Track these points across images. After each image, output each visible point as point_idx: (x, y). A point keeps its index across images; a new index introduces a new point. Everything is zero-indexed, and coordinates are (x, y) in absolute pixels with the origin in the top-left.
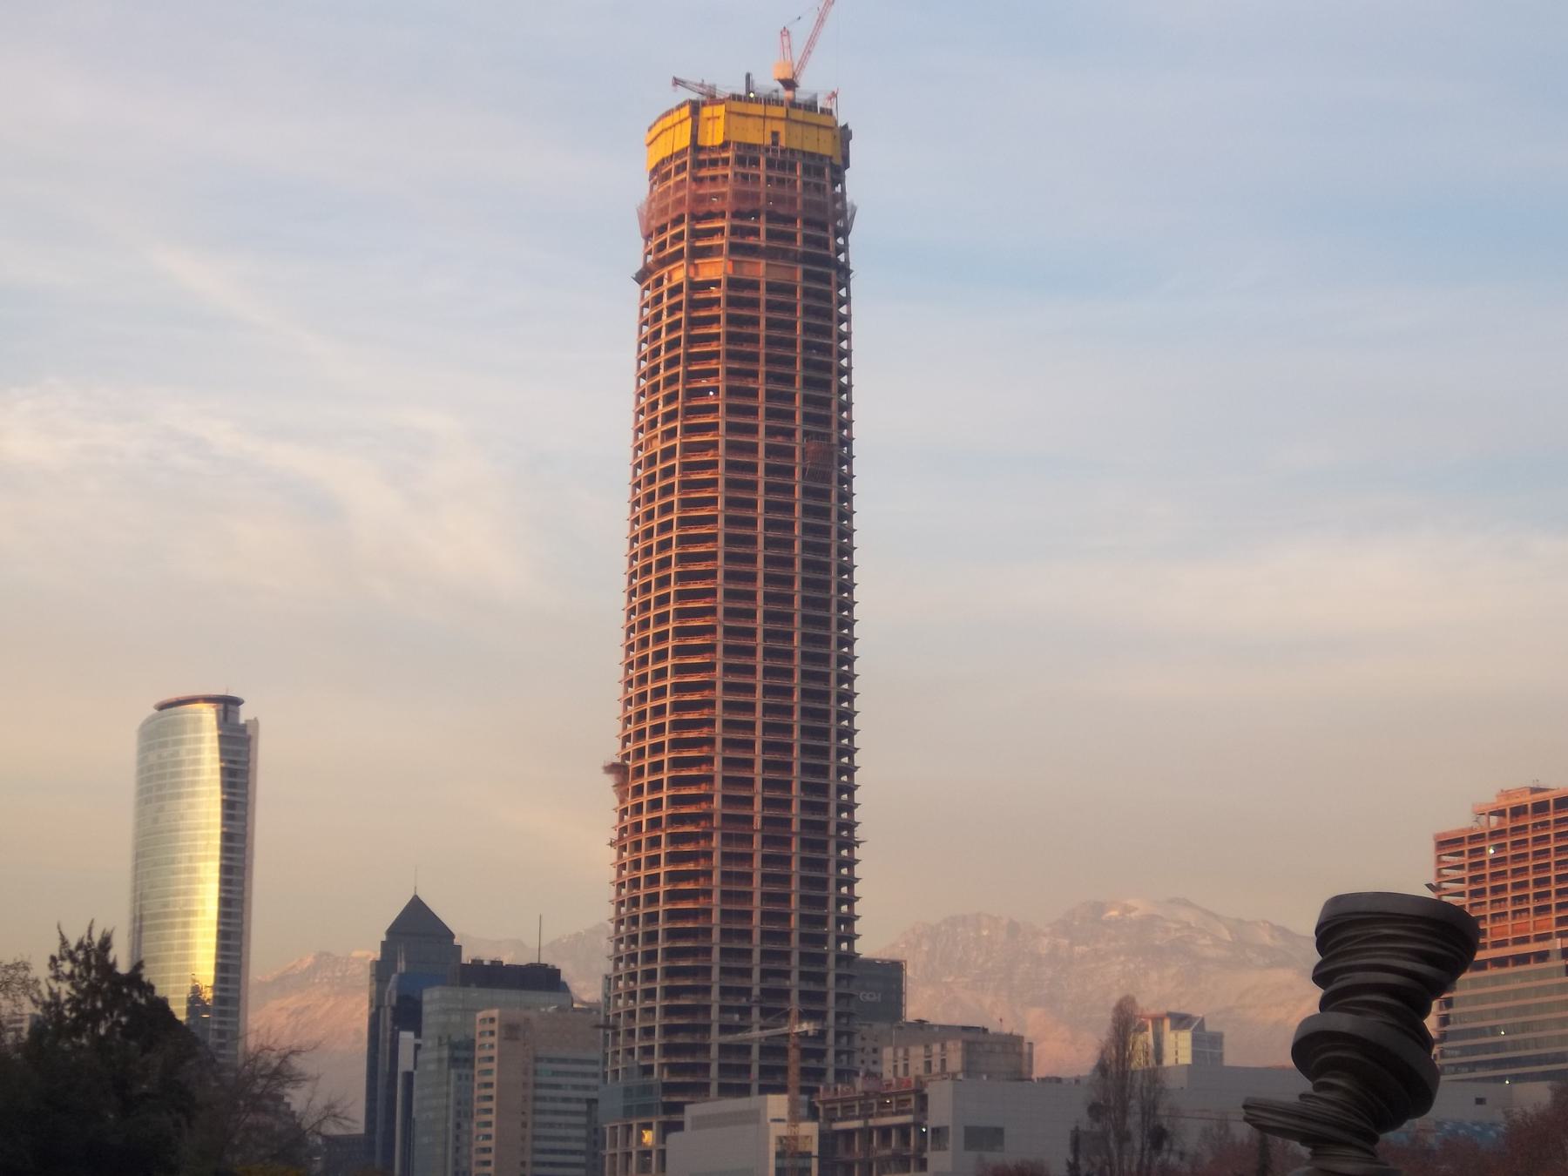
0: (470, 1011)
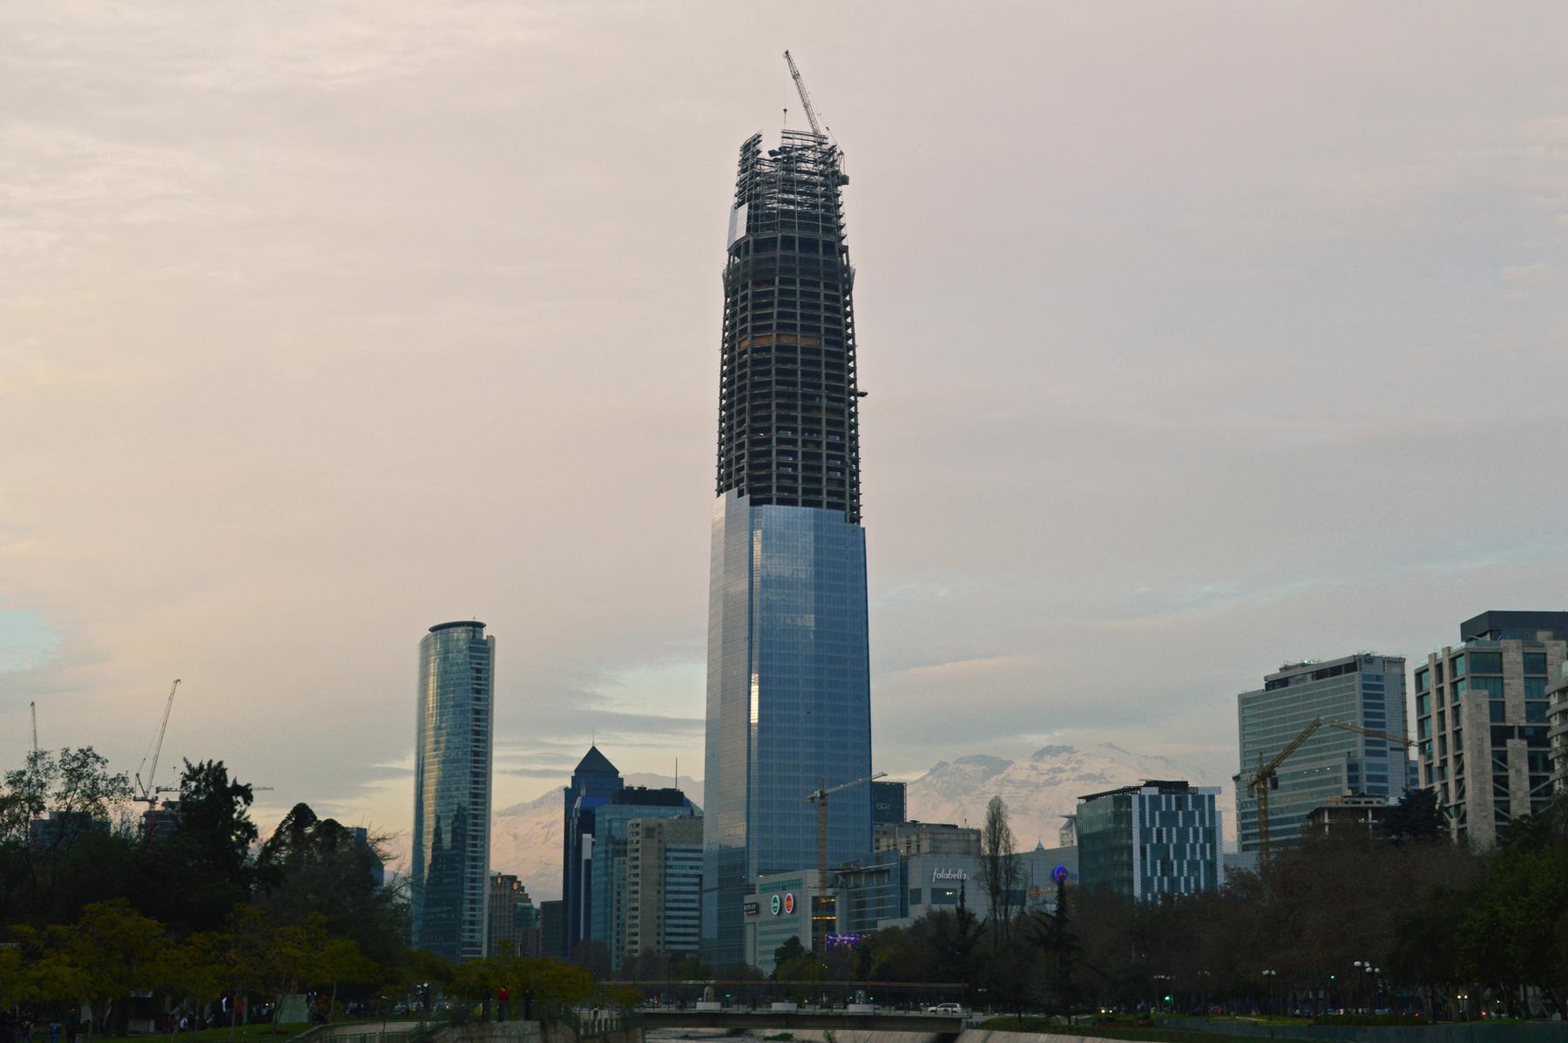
0: (623, 820)
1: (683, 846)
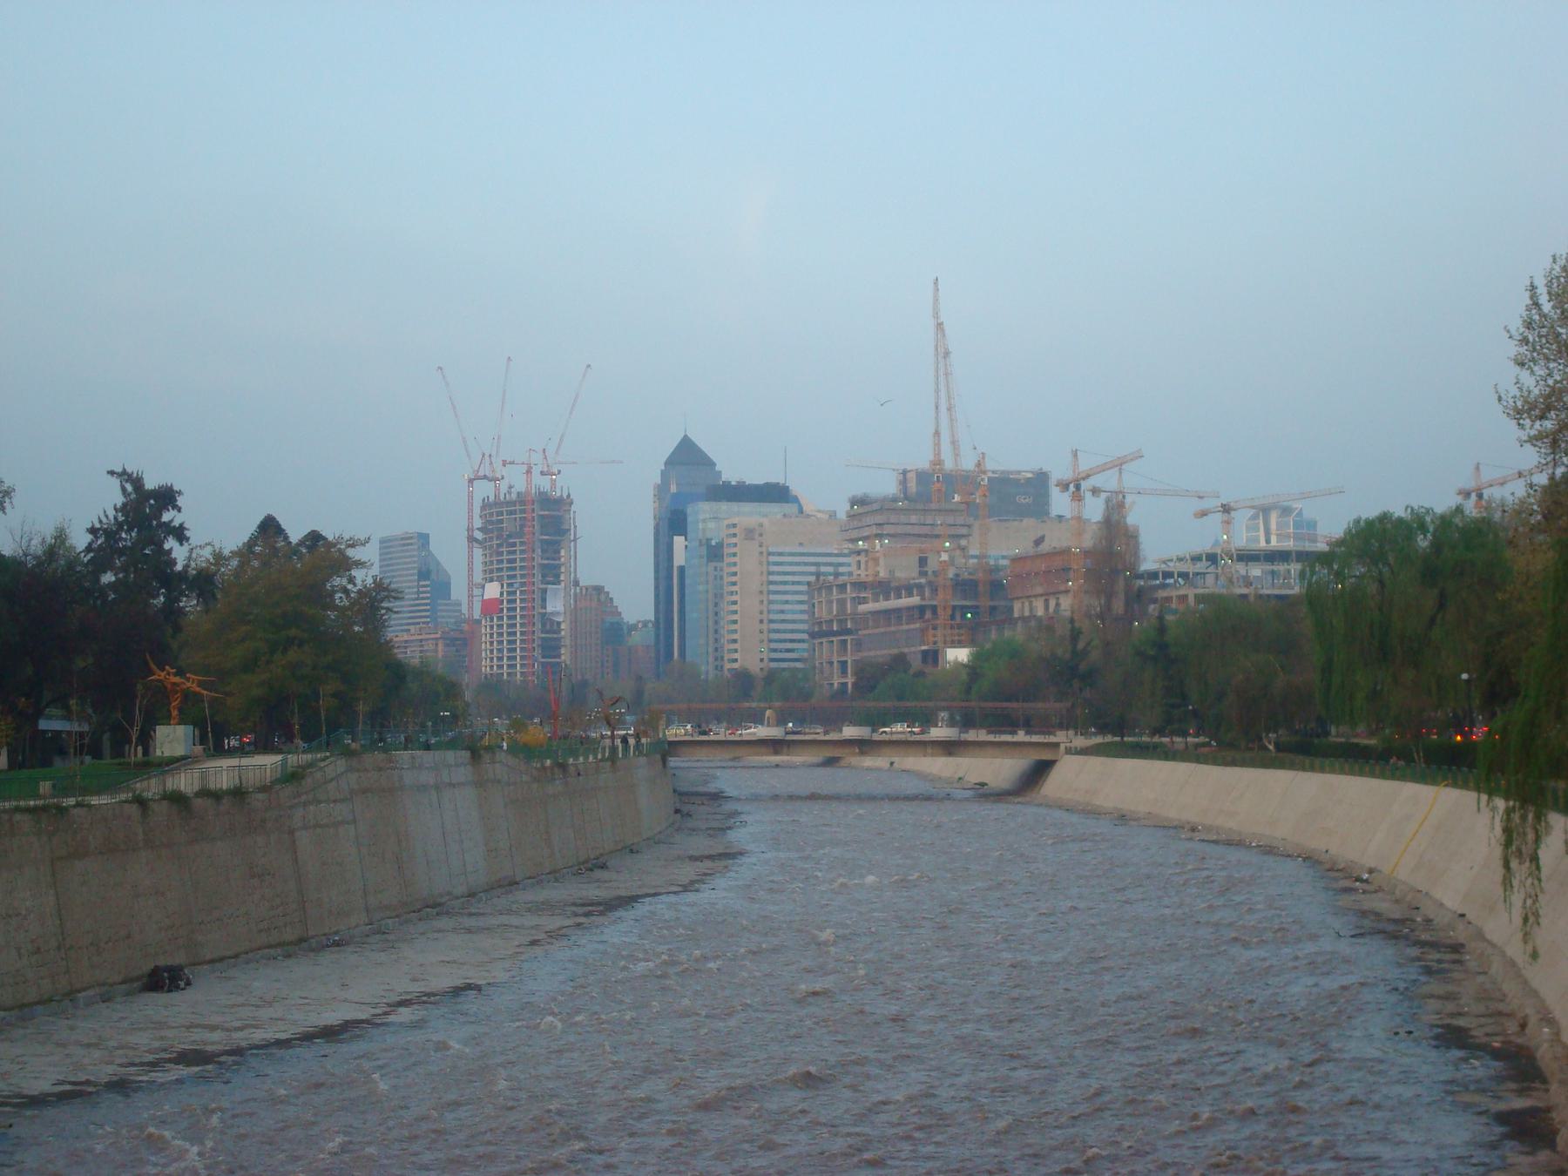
1: (819, 550)
